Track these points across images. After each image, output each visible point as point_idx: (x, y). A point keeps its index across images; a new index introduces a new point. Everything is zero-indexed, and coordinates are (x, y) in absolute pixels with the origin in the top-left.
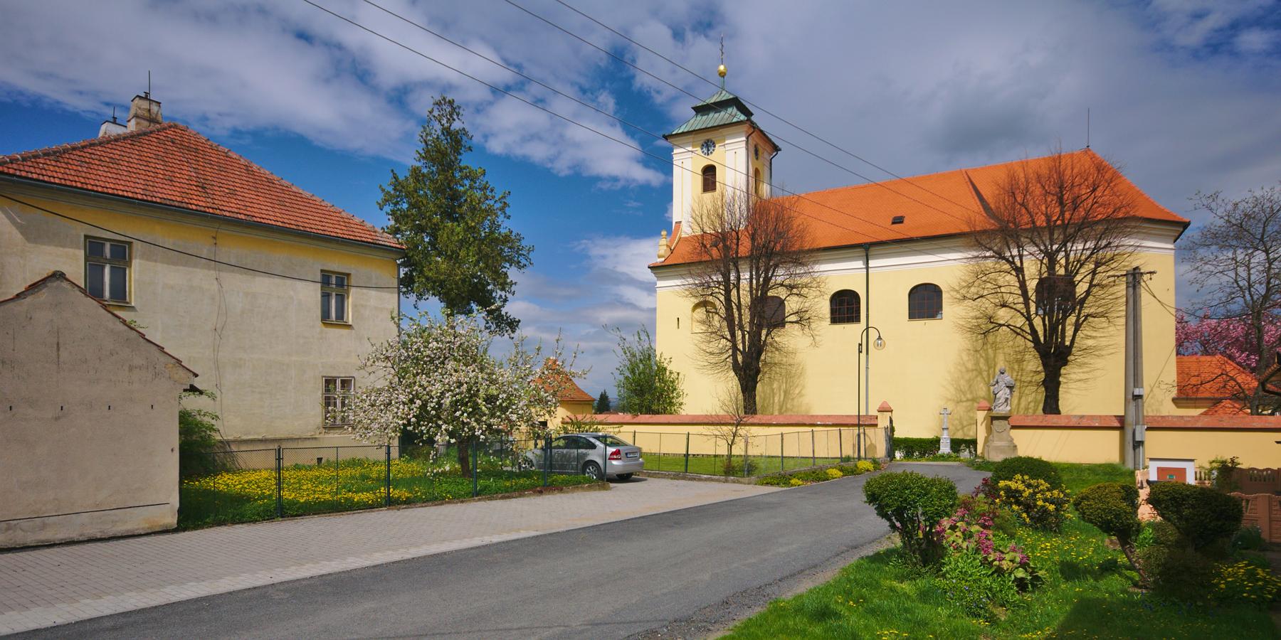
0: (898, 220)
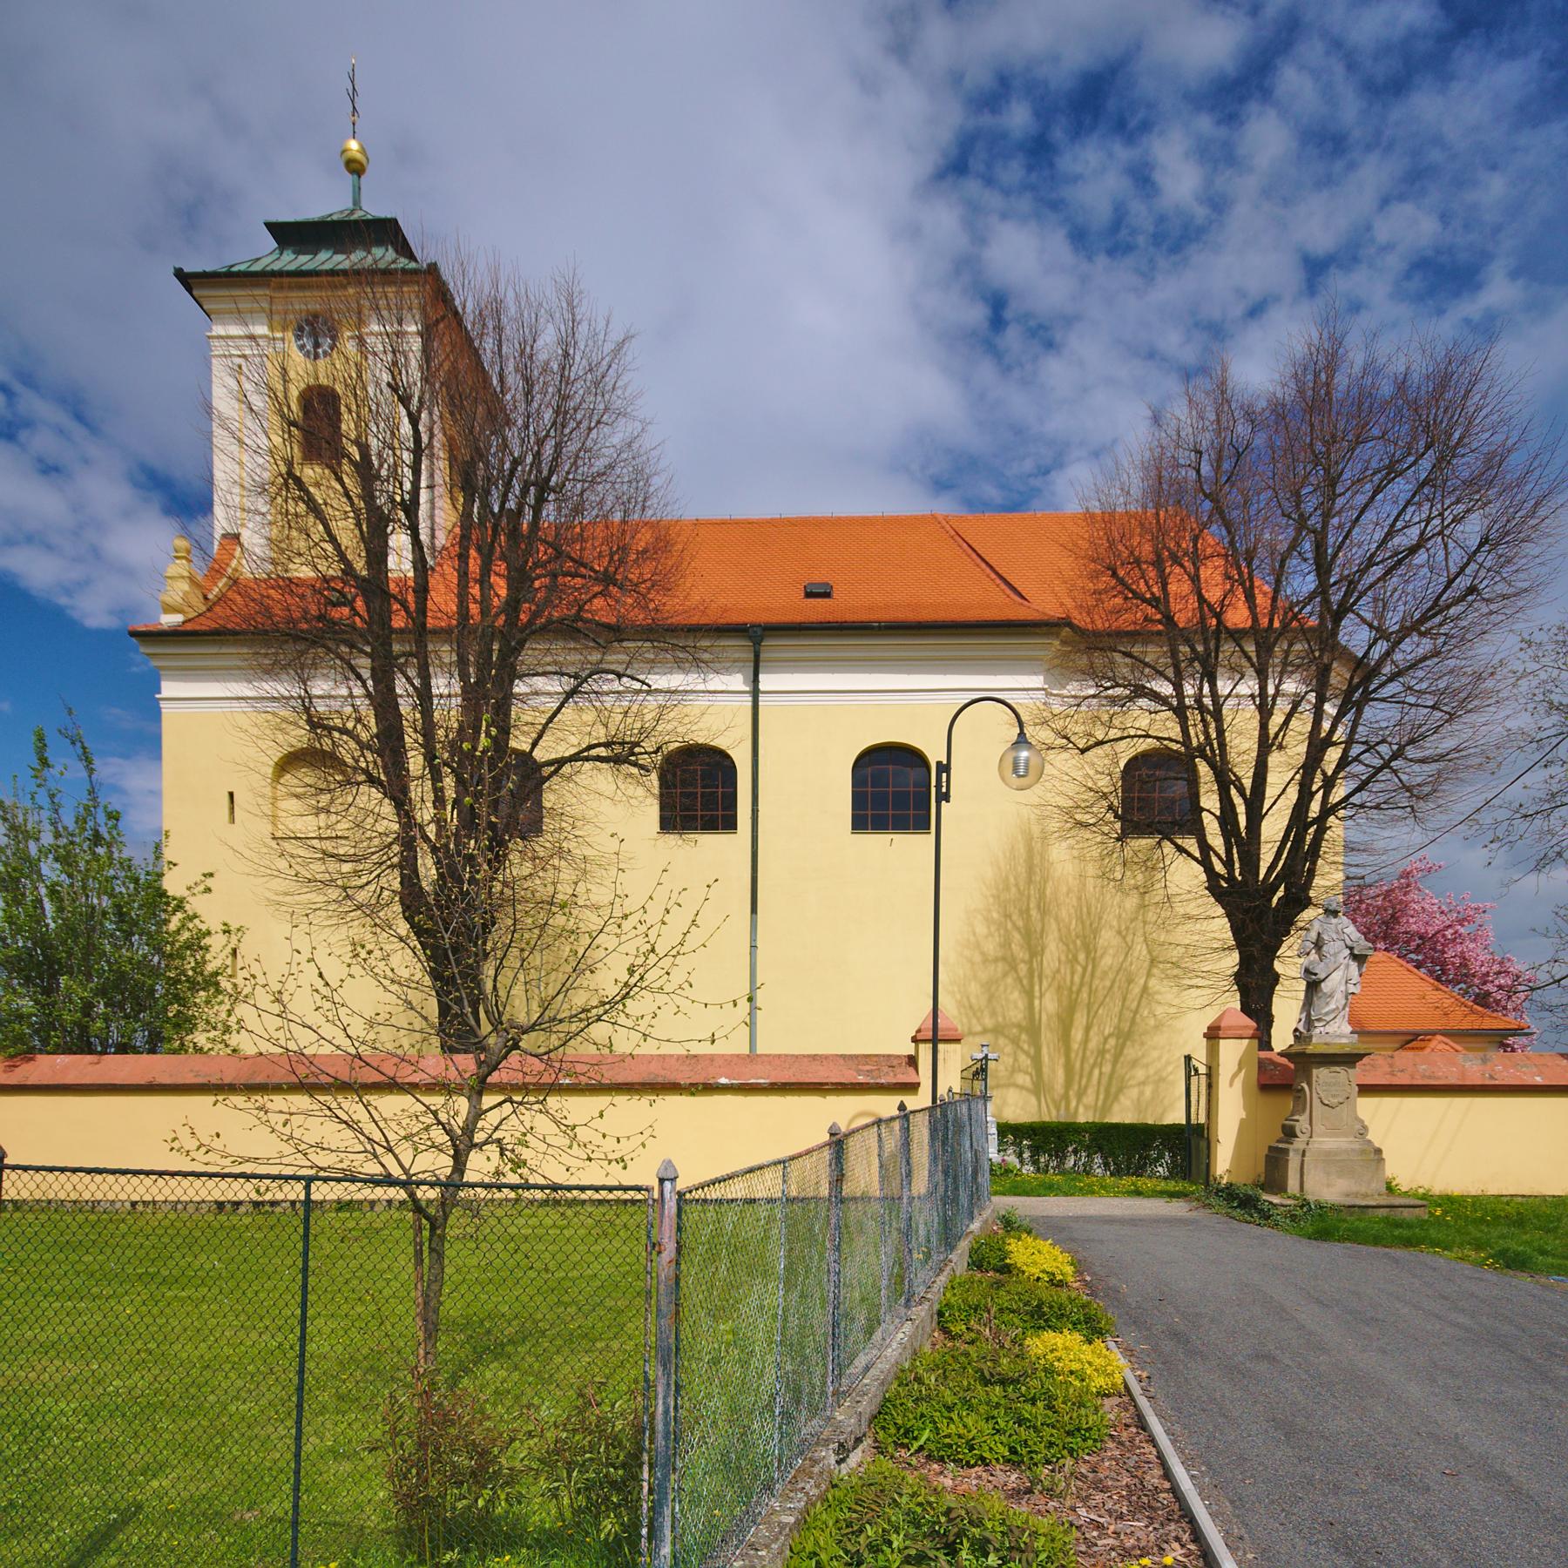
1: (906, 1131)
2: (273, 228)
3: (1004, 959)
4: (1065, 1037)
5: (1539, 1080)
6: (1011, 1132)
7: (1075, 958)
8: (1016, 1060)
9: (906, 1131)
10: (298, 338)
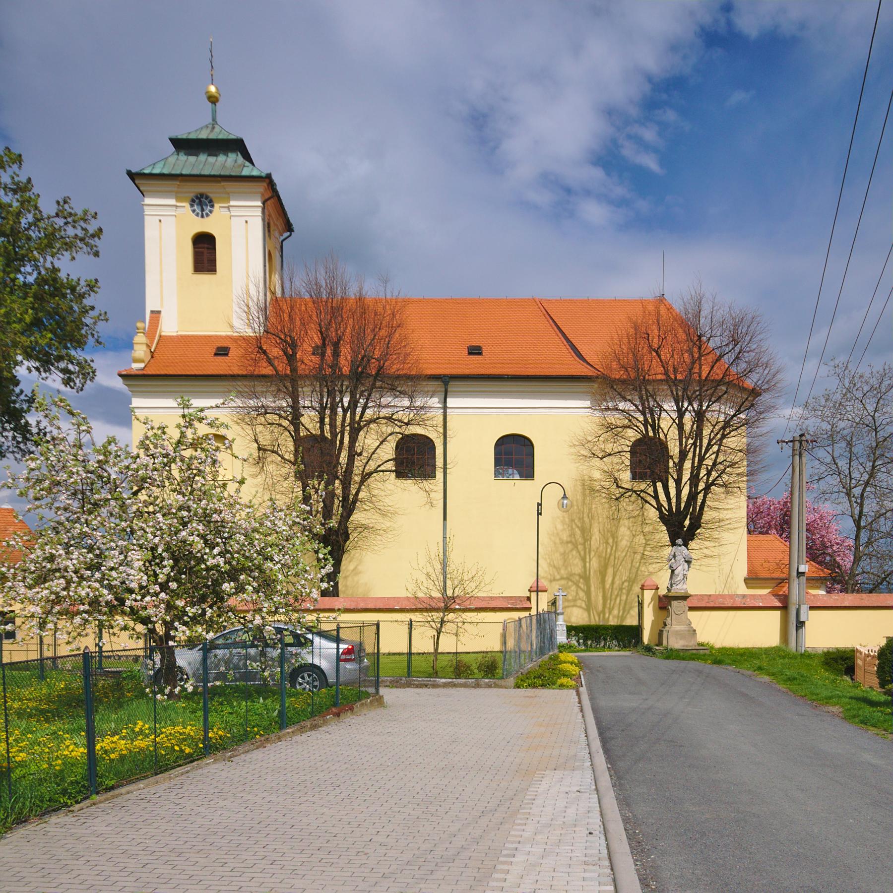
0: (475, 351)
1: (531, 620)
2: (173, 140)
3: (571, 542)
4: (603, 582)
5: (761, 605)
6: (572, 630)
7: (607, 543)
8: (577, 593)
9: (531, 620)
10: (192, 206)
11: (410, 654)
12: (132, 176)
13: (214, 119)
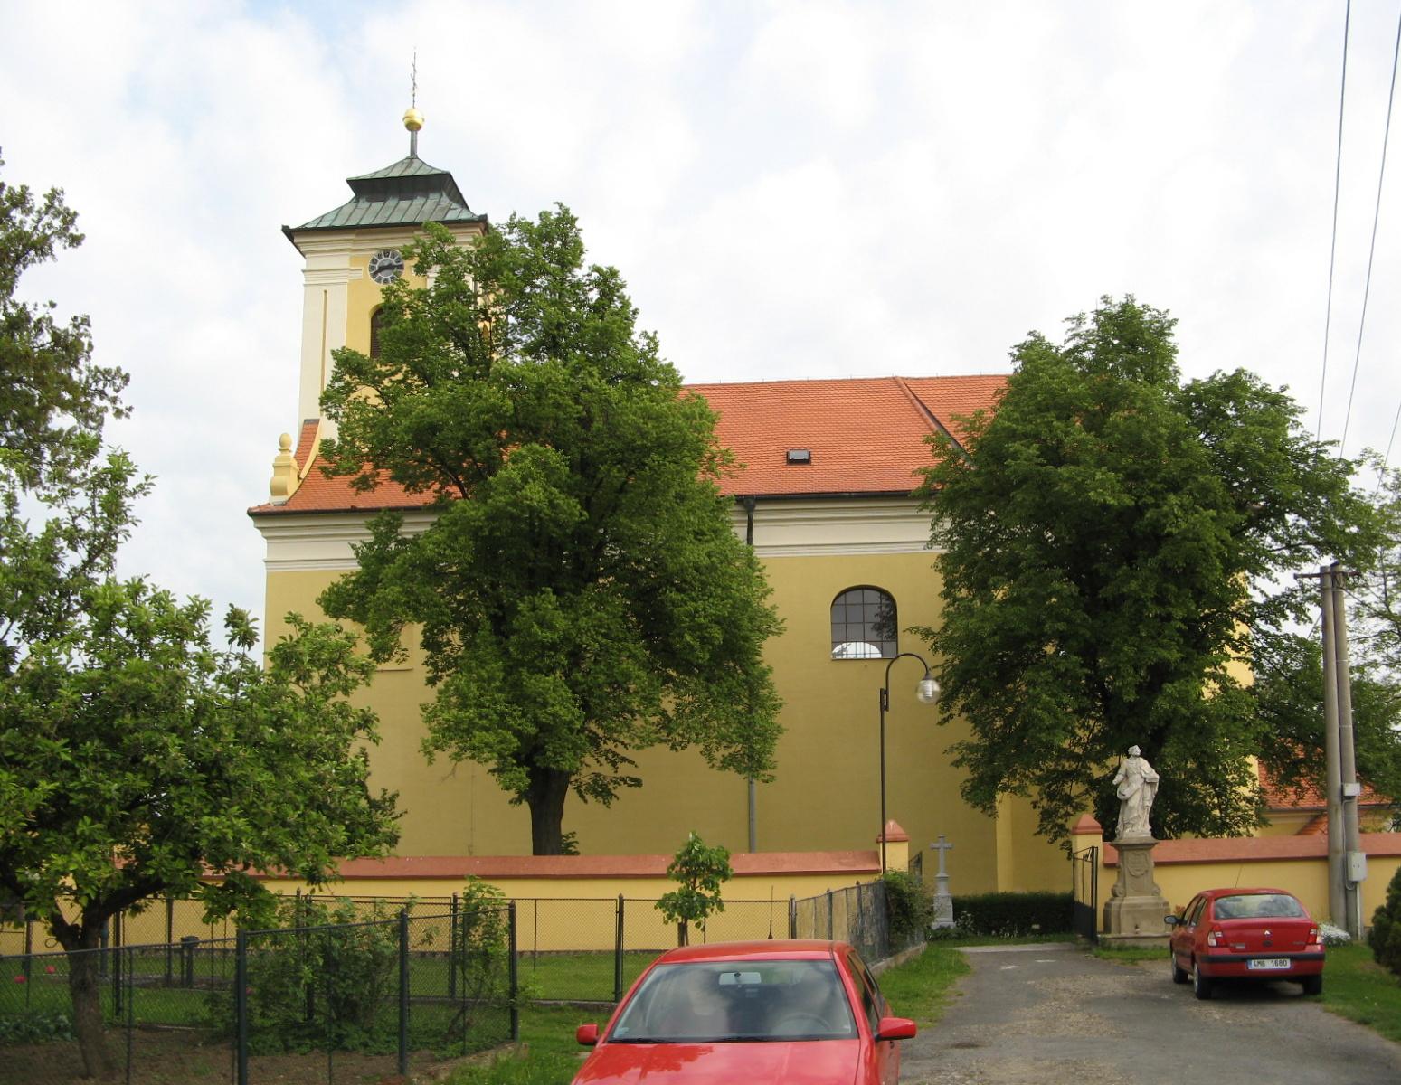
11: (619, 954)
12: (290, 233)
13: (413, 151)
